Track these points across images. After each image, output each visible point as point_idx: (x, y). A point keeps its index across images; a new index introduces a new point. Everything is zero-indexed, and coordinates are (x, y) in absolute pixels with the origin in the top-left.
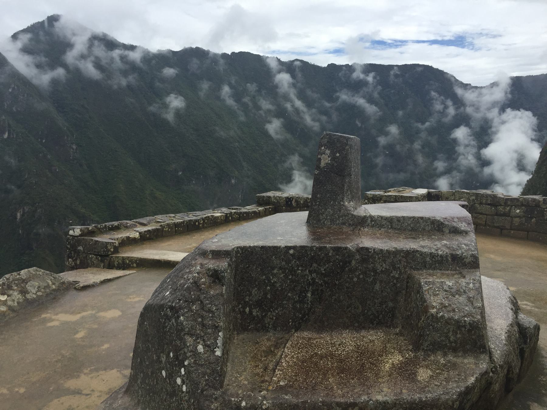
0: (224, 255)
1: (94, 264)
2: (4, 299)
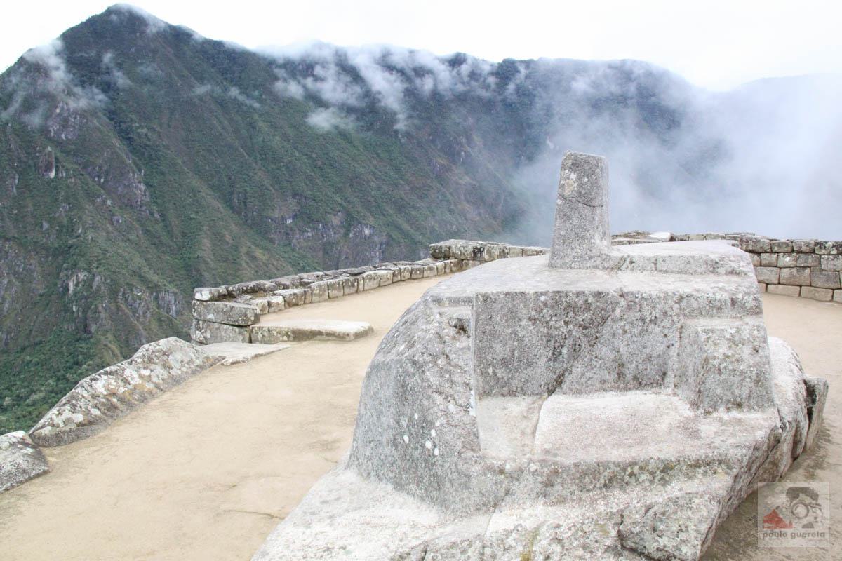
0: (465, 302)
1: (230, 337)
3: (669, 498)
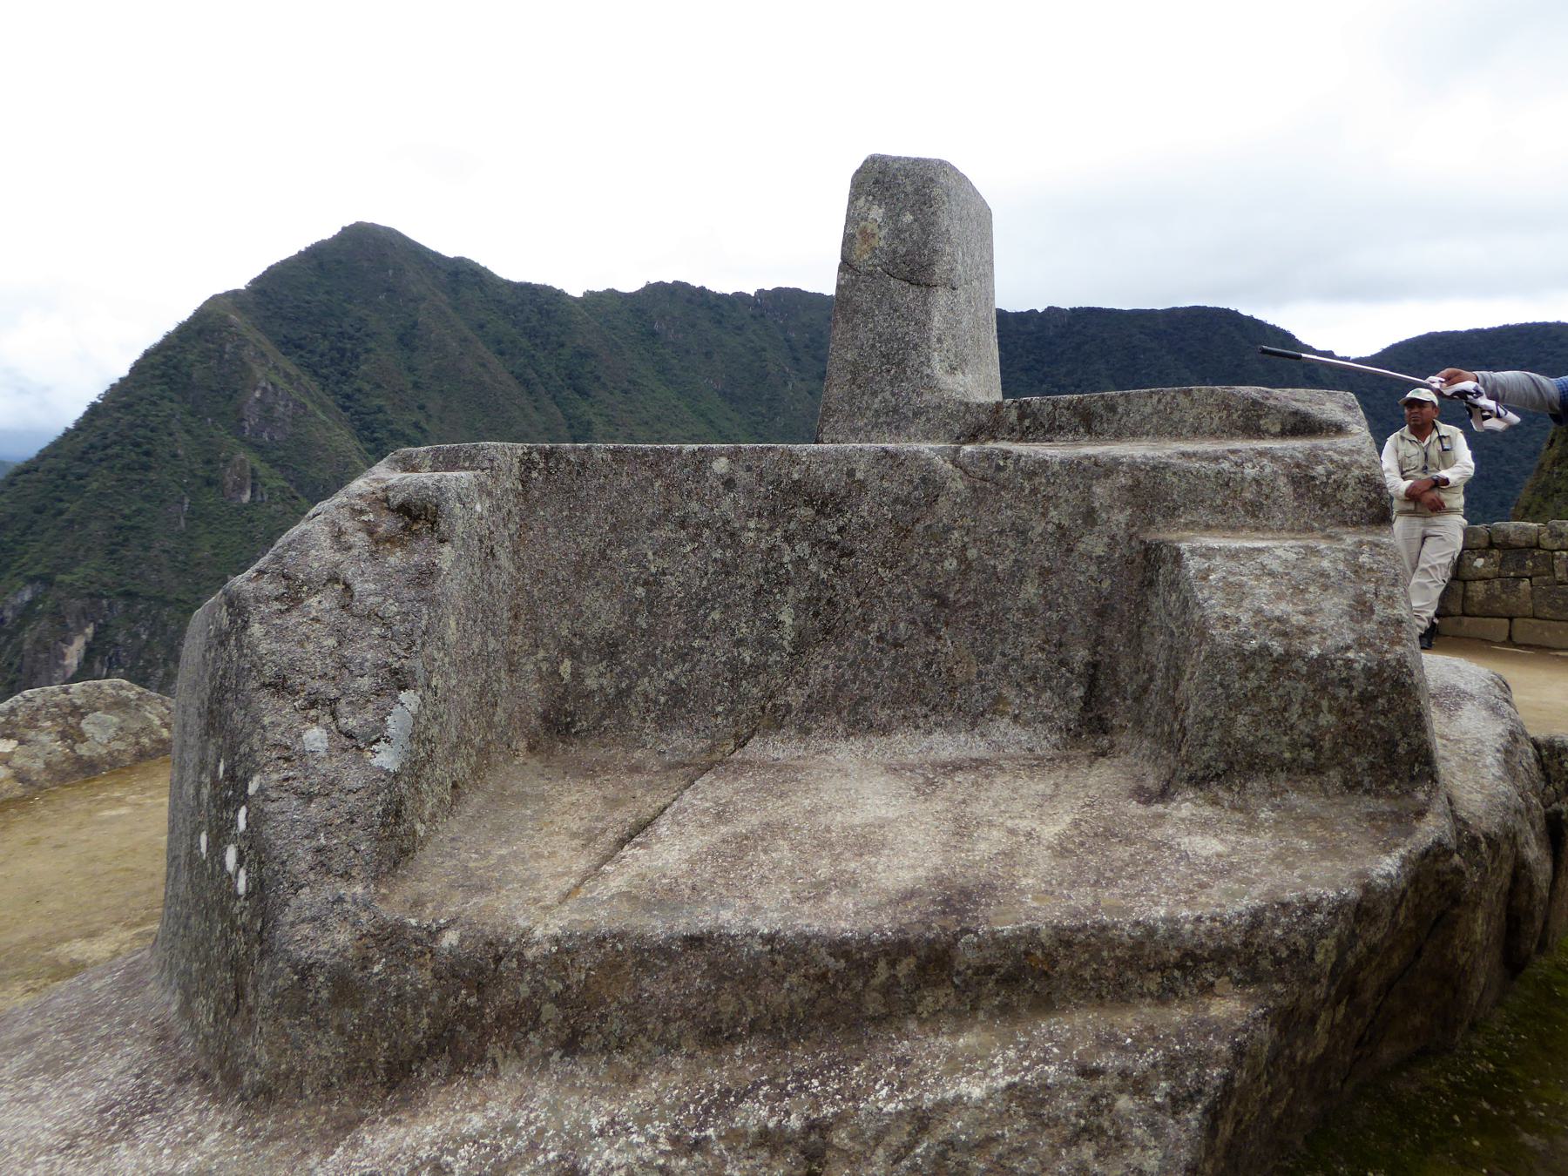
2: (8, 750)
3: (1011, 1086)
